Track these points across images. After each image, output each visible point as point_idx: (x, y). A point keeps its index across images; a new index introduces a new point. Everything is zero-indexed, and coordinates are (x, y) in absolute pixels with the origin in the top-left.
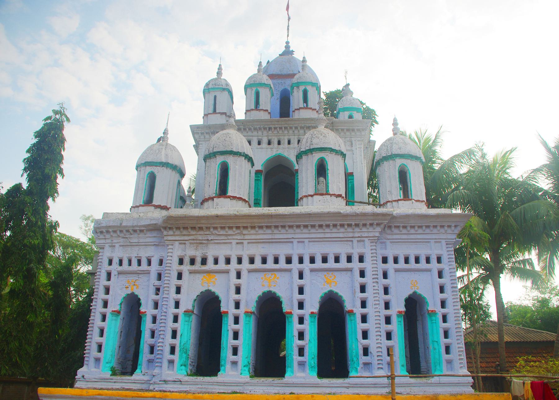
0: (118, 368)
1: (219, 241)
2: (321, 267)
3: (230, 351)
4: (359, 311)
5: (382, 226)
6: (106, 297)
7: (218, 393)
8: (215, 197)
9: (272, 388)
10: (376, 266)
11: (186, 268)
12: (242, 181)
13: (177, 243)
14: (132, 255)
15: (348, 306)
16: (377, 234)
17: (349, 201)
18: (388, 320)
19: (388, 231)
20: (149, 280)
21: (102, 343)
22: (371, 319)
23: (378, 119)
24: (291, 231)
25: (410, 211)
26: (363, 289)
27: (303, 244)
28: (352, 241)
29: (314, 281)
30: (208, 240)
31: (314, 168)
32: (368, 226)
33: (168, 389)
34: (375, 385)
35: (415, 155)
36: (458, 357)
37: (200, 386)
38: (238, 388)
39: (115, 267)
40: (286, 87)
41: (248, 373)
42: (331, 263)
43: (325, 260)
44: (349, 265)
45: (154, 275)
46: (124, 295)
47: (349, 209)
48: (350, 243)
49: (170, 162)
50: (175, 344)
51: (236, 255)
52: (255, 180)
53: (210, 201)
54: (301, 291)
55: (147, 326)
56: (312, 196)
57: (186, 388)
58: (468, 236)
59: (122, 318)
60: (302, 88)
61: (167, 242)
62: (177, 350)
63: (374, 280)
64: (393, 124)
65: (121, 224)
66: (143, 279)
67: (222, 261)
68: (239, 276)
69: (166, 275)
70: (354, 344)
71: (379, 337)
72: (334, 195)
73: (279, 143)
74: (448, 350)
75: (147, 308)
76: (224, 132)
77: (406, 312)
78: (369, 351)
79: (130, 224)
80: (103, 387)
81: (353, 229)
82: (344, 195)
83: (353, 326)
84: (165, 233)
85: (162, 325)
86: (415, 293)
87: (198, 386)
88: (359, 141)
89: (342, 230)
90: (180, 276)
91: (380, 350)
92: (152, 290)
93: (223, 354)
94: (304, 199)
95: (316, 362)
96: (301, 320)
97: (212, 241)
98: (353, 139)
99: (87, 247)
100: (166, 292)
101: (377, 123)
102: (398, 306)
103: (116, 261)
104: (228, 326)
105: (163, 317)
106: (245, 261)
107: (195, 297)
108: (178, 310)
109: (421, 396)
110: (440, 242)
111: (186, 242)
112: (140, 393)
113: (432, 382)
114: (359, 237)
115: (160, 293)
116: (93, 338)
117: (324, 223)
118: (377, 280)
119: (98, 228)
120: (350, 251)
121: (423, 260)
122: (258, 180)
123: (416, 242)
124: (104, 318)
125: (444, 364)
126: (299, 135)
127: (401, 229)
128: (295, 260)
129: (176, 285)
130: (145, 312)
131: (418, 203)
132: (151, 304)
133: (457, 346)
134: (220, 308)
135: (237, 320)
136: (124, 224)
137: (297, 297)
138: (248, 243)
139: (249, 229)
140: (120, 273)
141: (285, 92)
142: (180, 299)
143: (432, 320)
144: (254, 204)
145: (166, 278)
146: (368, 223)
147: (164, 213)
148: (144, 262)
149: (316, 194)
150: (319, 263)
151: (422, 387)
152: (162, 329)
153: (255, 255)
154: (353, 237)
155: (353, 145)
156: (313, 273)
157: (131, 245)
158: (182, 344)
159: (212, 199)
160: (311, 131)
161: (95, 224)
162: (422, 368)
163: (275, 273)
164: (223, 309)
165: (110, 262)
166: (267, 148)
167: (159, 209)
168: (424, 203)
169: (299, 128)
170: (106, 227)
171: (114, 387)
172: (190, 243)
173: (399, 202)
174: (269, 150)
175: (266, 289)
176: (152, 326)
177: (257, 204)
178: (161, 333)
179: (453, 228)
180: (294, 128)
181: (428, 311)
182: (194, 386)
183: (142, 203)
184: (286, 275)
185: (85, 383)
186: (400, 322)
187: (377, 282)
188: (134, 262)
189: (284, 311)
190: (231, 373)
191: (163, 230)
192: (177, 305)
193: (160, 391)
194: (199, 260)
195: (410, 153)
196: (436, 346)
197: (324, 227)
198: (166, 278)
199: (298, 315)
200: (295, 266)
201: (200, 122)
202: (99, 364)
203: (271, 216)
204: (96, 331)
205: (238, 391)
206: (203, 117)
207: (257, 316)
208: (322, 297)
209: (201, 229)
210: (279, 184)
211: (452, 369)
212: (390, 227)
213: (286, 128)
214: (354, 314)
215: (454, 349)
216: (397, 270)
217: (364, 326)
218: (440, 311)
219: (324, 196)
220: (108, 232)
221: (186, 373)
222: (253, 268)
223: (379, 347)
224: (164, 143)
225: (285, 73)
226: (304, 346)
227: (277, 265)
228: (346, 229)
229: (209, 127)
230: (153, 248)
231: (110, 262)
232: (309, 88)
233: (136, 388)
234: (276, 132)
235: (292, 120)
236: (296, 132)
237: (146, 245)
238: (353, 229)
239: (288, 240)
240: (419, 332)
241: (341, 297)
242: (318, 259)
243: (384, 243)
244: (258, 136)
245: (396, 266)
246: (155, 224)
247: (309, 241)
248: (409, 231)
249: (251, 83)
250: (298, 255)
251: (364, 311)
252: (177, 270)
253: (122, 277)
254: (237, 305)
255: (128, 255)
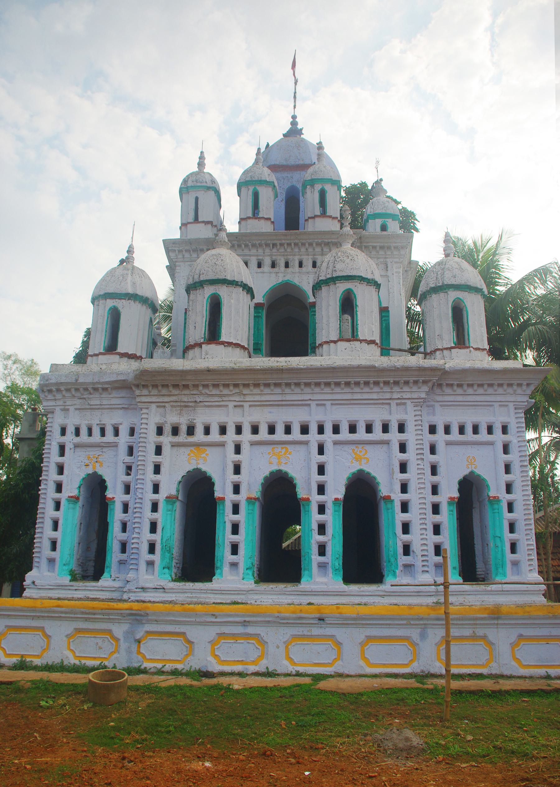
0: (78, 571)
1: (210, 404)
2: (349, 439)
3: (228, 549)
4: (398, 497)
5: (430, 384)
6: (59, 478)
7: (214, 603)
8: (203, 343)
9: (284, 597)
10: (420, 437)
11: (166, 439)
12: (238, 321)
13: (154, 406)
14: (93, 422)
15: (383, 491)
16: (423, 395)
17: (385, 350)
18: (436, 509)
19: (438, 391)
20: (116, 455)
21: (57, 539)
22: (414, 507)
23: (418, 225)
24: (307, 390)
25: (468, 365)
26: (403, 468)
27: (323, 407)
28: (389, 404)
29: (337, 457)
30: (196, 402)
31: (338, 304)
32: (411, 385)
33: (147, 599)
34: (418, 594)
35: (475, 286)
36: (527, 558)
37: (190, 595)
38: (239, 597)
39: (70, 439)
40: (294, 183)
41: (252, 577)
42: (361, 434)
43: (353, 429)
44: (386, 437)
45: (123, 449)
46: (83, 475)
47: (384, 362)
48: (387, 407)
49: (139, 293)
50: (155, 541)
51: (234, 423)
52: (255, 317)
53: (196, 349)
54: (321, 470)
55: (116, 516)
56: (335, 342)
57: (171, 597)
58: (542, 391)
59: (81, 506)
60: (318, 187)
61: (140, 405)
62: (158, 547)
63: (419, 457)
64: (444, 242)
65: (77, 380)
66: (108, 454)
67: (215, 430)
68: (238, 449)
69: (140, 449)
70: (391, 540)
71: (424, 532)
72: (365, 341)
73: (287, 265)
74: (513, 548)
75: (115, 492)
76: (213, 252)
77: (459, 499)
78: (411, 550)
79: (89, 380)
80: (61, 596)
81: (392, 388)
82: (378, 341)
83: (390, 518)
84: (138, 392)
85: (136, 515)
86: (472, 473)
87: (186, 595)
88: (396, 262)
89: (376, 389)
90: (159, 451)
91: (425, 548)
92: (122, 469)
93: (218, 553)
94: (324, 346)
95: (341, 564)
96: (322, 509)
97: (202, 404)
98: (388, 260)
99: (5, 399)
100: (140, 472)
101: (417, 230)
102: (450, 491)
103: (70, 430)
104: (225, 518)
105: (137, 505)
106: (247, 429)
107: (180, 478)
108: (157, 495)
109: (478, 607)
110: (507, 405)
111: (167, 405)
112: (112, 604)
113: (493, 589)
114: (399, 399)
115: (133, 473)
116: (44, 533)
117: (352, 380)
118: (422, 456)
119: (46, 385)
120: (386, 417)
121: (483, 430)
122: (258, 317)
123: (475, 405)
124: (58, 505)
125: (508, 566)
126: (314, 255)
127: (455, 388)
128: (313, 429)
129: (153, 462)
130: (113, 498)
131: (478, 352)
132: (120, 488)
133: (526, 543)
134: (295, 494)
135: (236, 509)
136: (81, 380)
137: (316, 478)
138: (250, 406)
139: (252, 388)
140: (76, 446)
141: (295, 194)
142: (160, 481)
143: (493, 509)
144: (254, 349)
145: (140, 453)
146: (411, 380)
147: (135, 365)
148: (109, 431)
149: (341, 339)
150: (345, 434)
151: (479, 596)
152: (137, 520)
153: (259, 422)
154: (390, 399)
155: (389, 269)
156: (337, 446)
157: (90, 409)
158: (164, 540)
159: (200, 345)
160: (334, 251)
161: (41, 380)
162: (478, 570)
163: (286, 446)
164: (217, 494)
165: (63, 432)
166: (270, 273)
167: (126, 359)
168: (485, 352)
169: (314, 245)
170: (57, 384)
171: (75, 596)
172: (172, 406)
173: (452, 350)
174: (273, 275)
175: (274, 468)
176: (122, 516)
177: (257, 349)
178: (136, 525)
179: (524, 387)
180: (307, 245)
181: (489, 497)
182: (182, 595)
183: (102, 351)
184: (302, 448)
185: (36, 591)
186: (452, 511)
187: (423, 459)
188: (96, 431)
189: (299, 497)
190: (230, 578)
191: (134, 388)
192: (156, 489)
193: (138, 601)
194: (183, 429)
195: (468, 284)
196: (499, 543)
197: (353, 386)
198: (140, 453)
199: (317, 502)
200: (313, 437)
201: (177, 235)
202: (54, 565)
203: (280, 371)
204: (48, 524)
205: (240, 601)
206: (180, 228)
207: (261, 503)
208: (349, 479)
209: (186, 387)
210: (287, 324)
211: (518, 573)
212: (440, 385)
213: (296, 244)
214: (392, 501)
215: (522, 547)
216: (448, 443)
217: (405, 517)
218: (505, 497)
219: (351, 343)
220: (58, 390)
221: (170, 578)
222: (466, 439)
223: (425, 544)
224: (129, 266)
225: (293, 163)
226: (326, 542)
227: (289, 436)
228: (382, 388)
229: (190, 242)
230: (121, 412)
231: (63, 432)
232: (328, 188)
233: (104, 597)
234: (282, 250)
235: (305, 233)
236: (310, 250)
237: (111, 408)
238: (392, 388)
239: (303, 403)
240: (474, 524)
241: (374, 478)
242: (344, 428)
243: (432, 406)
244: (257, 256)
245: (448, 437)
246: (124, 380)
247: (332, 404)
248: (465, 391)
249: (247, 179)
250: (318, 422)
251: (405, 497)
252: (155, 442)
253: (80, 452)
254: (237, 489)
255: (87, 422)
